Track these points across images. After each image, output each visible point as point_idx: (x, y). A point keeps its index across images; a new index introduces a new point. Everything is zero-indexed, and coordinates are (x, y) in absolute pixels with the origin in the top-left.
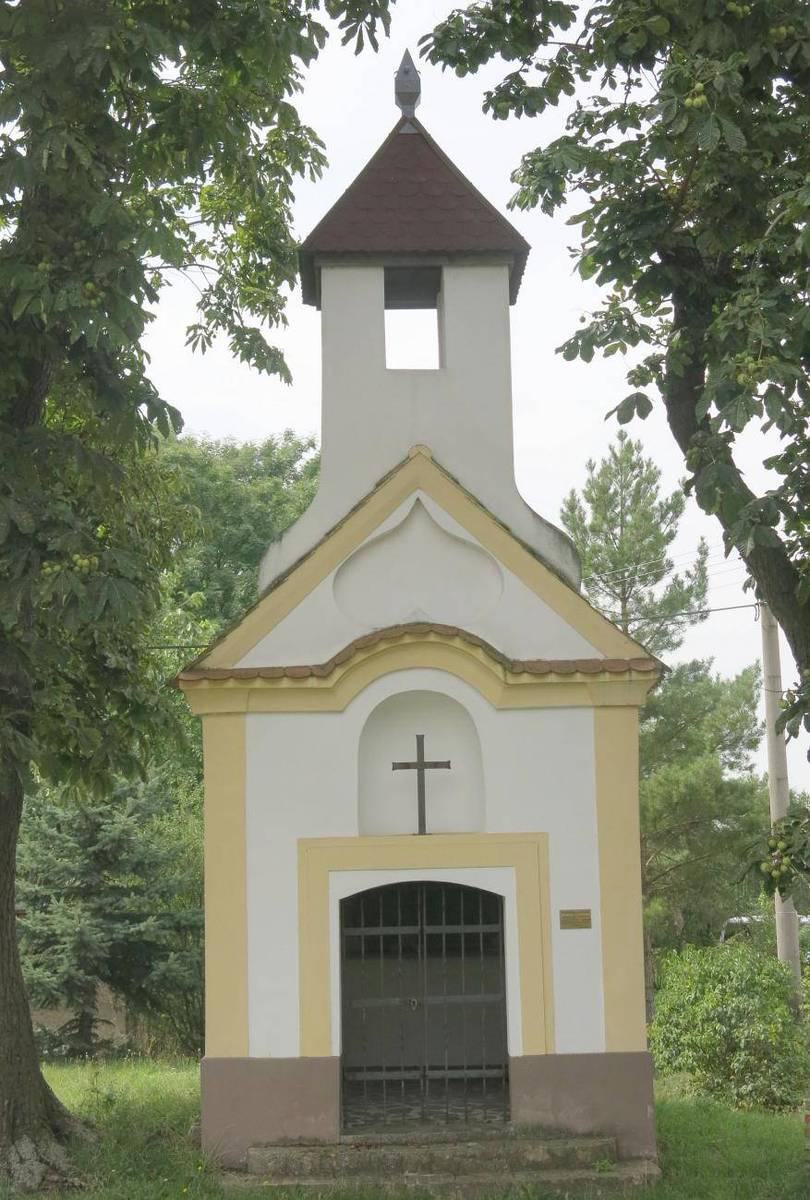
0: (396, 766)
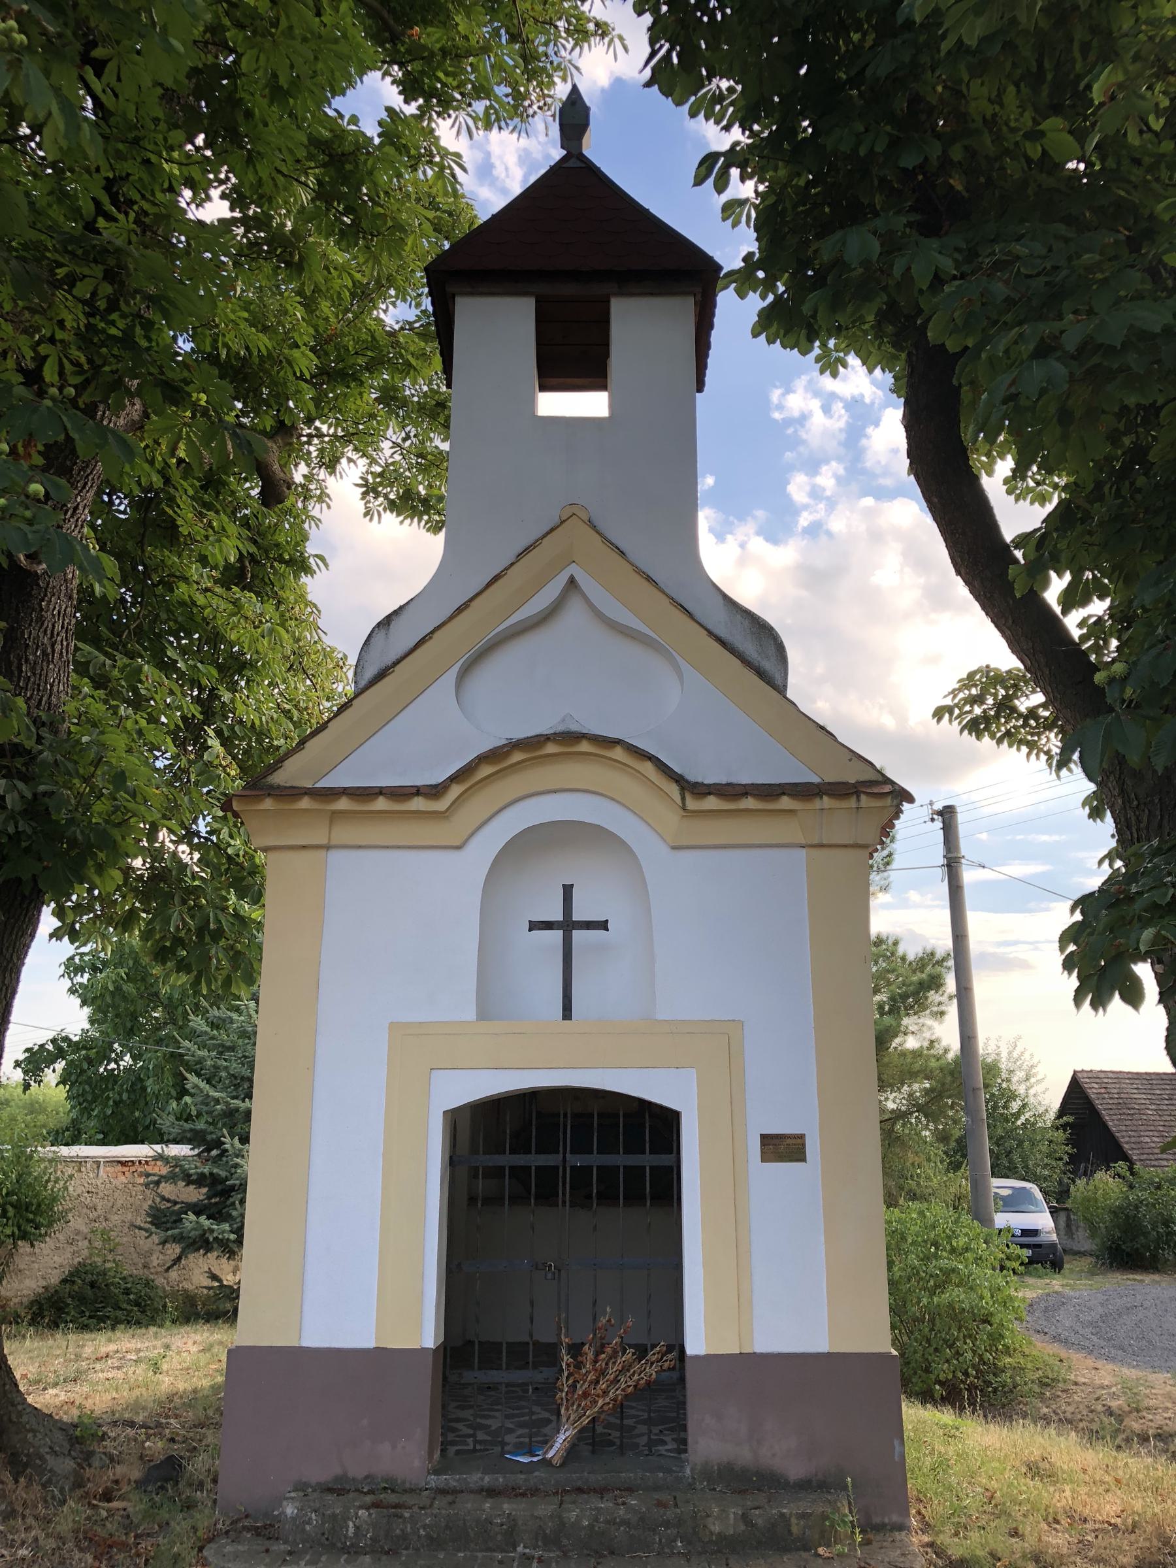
0: (534, 926)
